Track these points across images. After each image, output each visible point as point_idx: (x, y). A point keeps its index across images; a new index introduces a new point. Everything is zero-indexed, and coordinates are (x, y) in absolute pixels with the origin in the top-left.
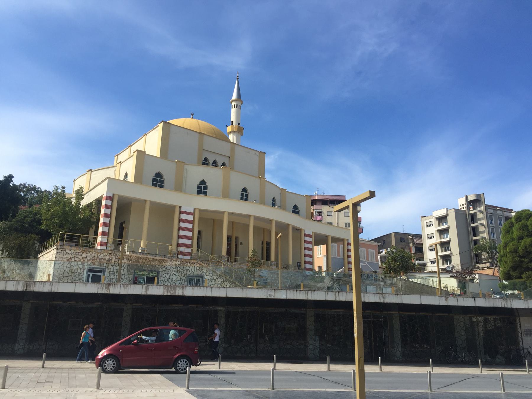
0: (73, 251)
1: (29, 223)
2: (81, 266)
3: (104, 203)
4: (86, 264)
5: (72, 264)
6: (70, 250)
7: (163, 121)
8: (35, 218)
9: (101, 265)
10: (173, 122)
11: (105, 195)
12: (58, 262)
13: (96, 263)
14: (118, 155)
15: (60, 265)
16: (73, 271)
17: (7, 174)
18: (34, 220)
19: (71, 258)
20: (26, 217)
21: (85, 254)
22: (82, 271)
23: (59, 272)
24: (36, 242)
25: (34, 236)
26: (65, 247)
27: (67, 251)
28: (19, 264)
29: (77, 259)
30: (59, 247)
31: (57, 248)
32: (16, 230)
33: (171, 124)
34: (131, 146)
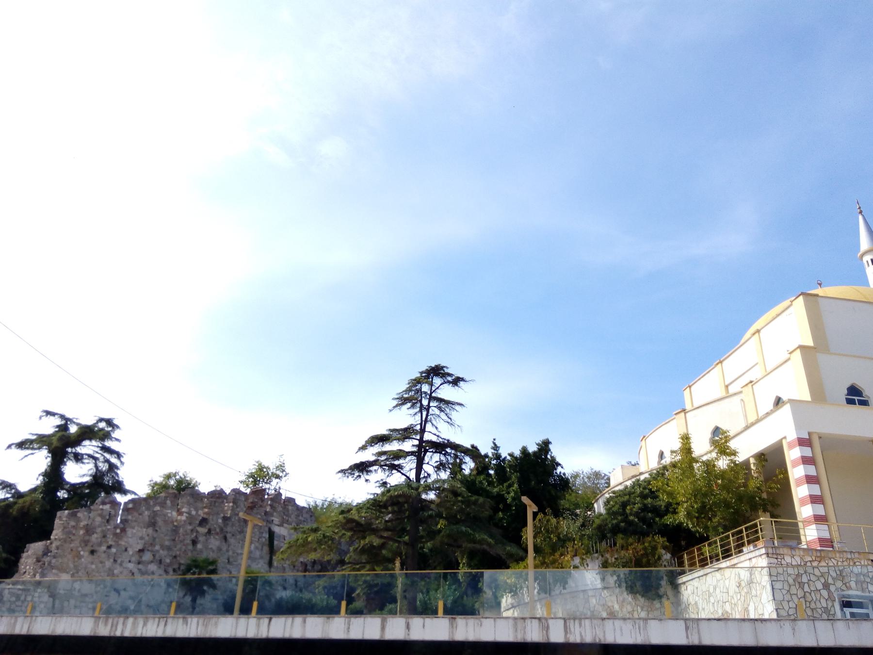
0: (798, 559)
1: (636, 515)
2: (825, 593)
3: (793, 454)
4: (832, 588)
5: (806, 588)
6: (793, 557)
7: (802, 294)
8: (645, 505)
9: (863, 590)
10: (819, 291)
11: (792, 435)
12: (778, 585)
13: (853, 584)
14: (690, 387)
15: (784, 592)
16: (813, 605)
17: (540, 439)
18: (645, 508)
19: (799, 575)
20: (624, 505)
21: (823, 564)
22: (830, 604)
23: (787, 608)
24: (663, 552)
25: (660, 540)
26: (781, 551)
27: (788, 559)
28: (642, 600)
29: (813, 578)
30: (770, 551)
31: (767, 554)
32: (616, 530)
33: (817, 295)
34: (721, 362)
